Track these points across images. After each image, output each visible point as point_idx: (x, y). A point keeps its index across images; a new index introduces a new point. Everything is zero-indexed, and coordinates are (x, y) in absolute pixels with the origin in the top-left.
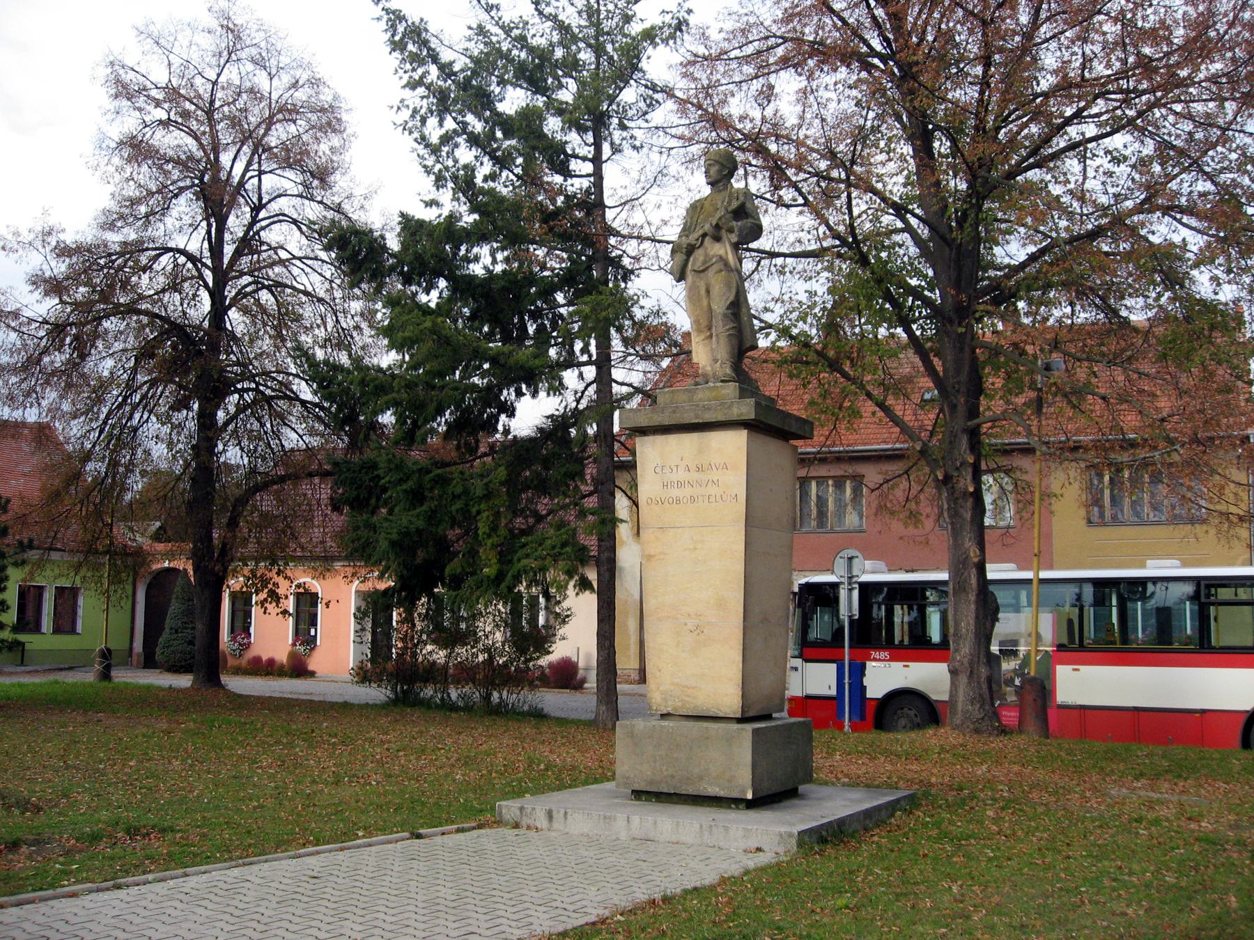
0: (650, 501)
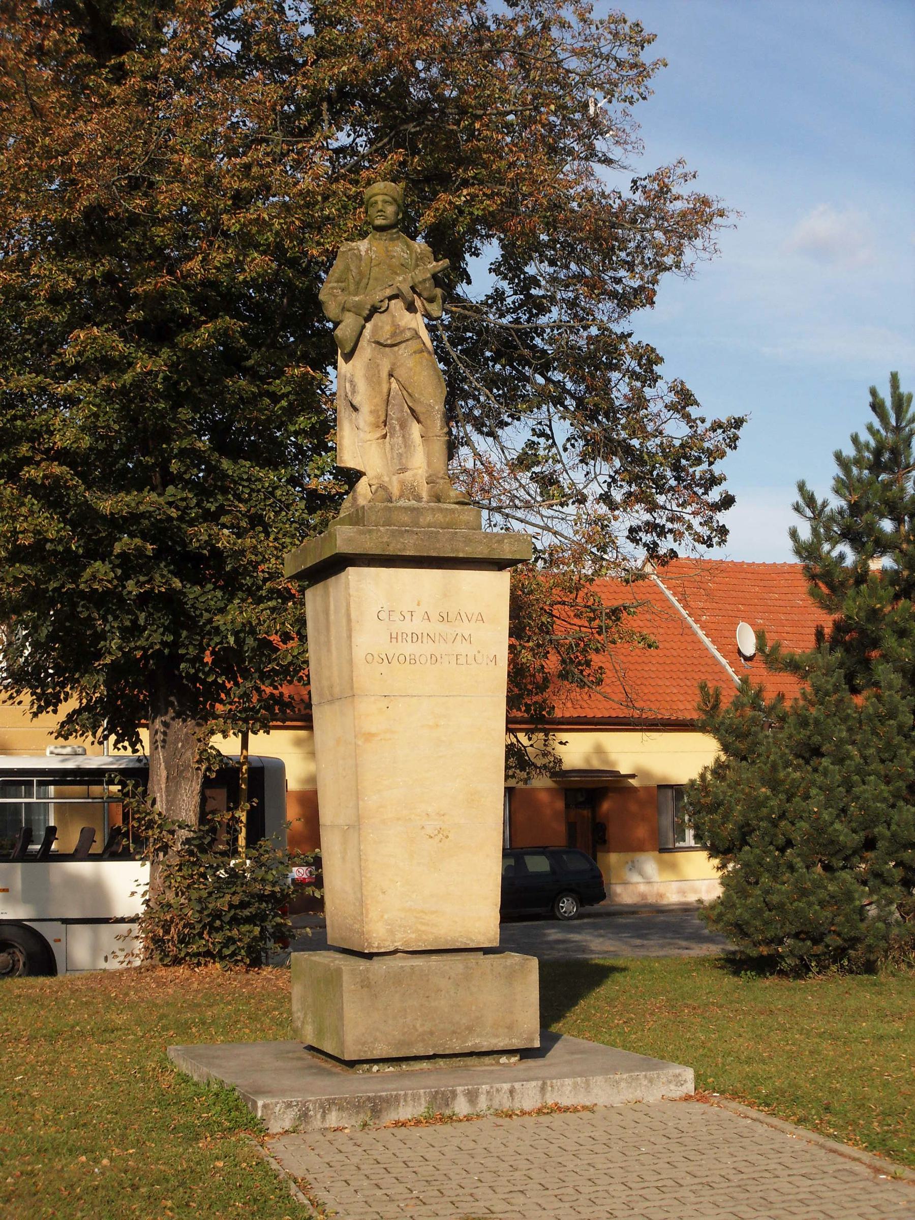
0: (370, 658)
